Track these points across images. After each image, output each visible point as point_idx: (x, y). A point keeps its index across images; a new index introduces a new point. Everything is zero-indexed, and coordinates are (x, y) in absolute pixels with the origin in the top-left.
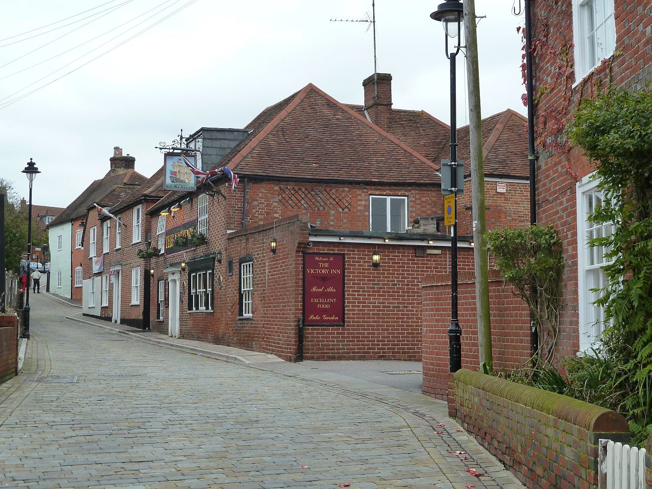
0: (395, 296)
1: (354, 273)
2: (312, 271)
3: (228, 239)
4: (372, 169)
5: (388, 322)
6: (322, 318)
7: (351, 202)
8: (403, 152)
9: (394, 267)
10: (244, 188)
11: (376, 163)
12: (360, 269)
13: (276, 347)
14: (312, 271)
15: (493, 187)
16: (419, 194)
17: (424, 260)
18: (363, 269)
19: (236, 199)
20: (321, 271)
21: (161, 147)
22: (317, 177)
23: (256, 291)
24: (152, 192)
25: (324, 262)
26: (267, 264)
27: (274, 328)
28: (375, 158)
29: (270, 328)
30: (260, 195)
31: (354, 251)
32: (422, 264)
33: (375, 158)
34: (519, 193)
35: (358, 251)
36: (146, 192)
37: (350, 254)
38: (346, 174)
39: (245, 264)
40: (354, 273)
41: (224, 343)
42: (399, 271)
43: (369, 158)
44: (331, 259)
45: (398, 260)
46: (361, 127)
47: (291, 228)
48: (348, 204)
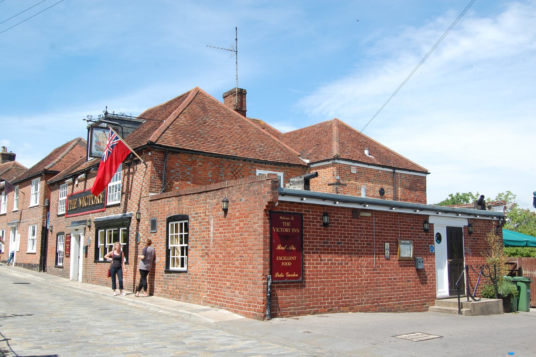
1: (309, 232)
2: (277, 230)
3: (150, 201)
4: (257, 151)
5: (334, 278)
6: (285, 275)
15: (348, 169)
16: (290, 172)
17: (358, 222)
19: (157, 167)
21: (89, 119)
34: (363, 175)
35: (312, 212)
36: (46, 168)
39: (174, 223)
44: (292, 219)
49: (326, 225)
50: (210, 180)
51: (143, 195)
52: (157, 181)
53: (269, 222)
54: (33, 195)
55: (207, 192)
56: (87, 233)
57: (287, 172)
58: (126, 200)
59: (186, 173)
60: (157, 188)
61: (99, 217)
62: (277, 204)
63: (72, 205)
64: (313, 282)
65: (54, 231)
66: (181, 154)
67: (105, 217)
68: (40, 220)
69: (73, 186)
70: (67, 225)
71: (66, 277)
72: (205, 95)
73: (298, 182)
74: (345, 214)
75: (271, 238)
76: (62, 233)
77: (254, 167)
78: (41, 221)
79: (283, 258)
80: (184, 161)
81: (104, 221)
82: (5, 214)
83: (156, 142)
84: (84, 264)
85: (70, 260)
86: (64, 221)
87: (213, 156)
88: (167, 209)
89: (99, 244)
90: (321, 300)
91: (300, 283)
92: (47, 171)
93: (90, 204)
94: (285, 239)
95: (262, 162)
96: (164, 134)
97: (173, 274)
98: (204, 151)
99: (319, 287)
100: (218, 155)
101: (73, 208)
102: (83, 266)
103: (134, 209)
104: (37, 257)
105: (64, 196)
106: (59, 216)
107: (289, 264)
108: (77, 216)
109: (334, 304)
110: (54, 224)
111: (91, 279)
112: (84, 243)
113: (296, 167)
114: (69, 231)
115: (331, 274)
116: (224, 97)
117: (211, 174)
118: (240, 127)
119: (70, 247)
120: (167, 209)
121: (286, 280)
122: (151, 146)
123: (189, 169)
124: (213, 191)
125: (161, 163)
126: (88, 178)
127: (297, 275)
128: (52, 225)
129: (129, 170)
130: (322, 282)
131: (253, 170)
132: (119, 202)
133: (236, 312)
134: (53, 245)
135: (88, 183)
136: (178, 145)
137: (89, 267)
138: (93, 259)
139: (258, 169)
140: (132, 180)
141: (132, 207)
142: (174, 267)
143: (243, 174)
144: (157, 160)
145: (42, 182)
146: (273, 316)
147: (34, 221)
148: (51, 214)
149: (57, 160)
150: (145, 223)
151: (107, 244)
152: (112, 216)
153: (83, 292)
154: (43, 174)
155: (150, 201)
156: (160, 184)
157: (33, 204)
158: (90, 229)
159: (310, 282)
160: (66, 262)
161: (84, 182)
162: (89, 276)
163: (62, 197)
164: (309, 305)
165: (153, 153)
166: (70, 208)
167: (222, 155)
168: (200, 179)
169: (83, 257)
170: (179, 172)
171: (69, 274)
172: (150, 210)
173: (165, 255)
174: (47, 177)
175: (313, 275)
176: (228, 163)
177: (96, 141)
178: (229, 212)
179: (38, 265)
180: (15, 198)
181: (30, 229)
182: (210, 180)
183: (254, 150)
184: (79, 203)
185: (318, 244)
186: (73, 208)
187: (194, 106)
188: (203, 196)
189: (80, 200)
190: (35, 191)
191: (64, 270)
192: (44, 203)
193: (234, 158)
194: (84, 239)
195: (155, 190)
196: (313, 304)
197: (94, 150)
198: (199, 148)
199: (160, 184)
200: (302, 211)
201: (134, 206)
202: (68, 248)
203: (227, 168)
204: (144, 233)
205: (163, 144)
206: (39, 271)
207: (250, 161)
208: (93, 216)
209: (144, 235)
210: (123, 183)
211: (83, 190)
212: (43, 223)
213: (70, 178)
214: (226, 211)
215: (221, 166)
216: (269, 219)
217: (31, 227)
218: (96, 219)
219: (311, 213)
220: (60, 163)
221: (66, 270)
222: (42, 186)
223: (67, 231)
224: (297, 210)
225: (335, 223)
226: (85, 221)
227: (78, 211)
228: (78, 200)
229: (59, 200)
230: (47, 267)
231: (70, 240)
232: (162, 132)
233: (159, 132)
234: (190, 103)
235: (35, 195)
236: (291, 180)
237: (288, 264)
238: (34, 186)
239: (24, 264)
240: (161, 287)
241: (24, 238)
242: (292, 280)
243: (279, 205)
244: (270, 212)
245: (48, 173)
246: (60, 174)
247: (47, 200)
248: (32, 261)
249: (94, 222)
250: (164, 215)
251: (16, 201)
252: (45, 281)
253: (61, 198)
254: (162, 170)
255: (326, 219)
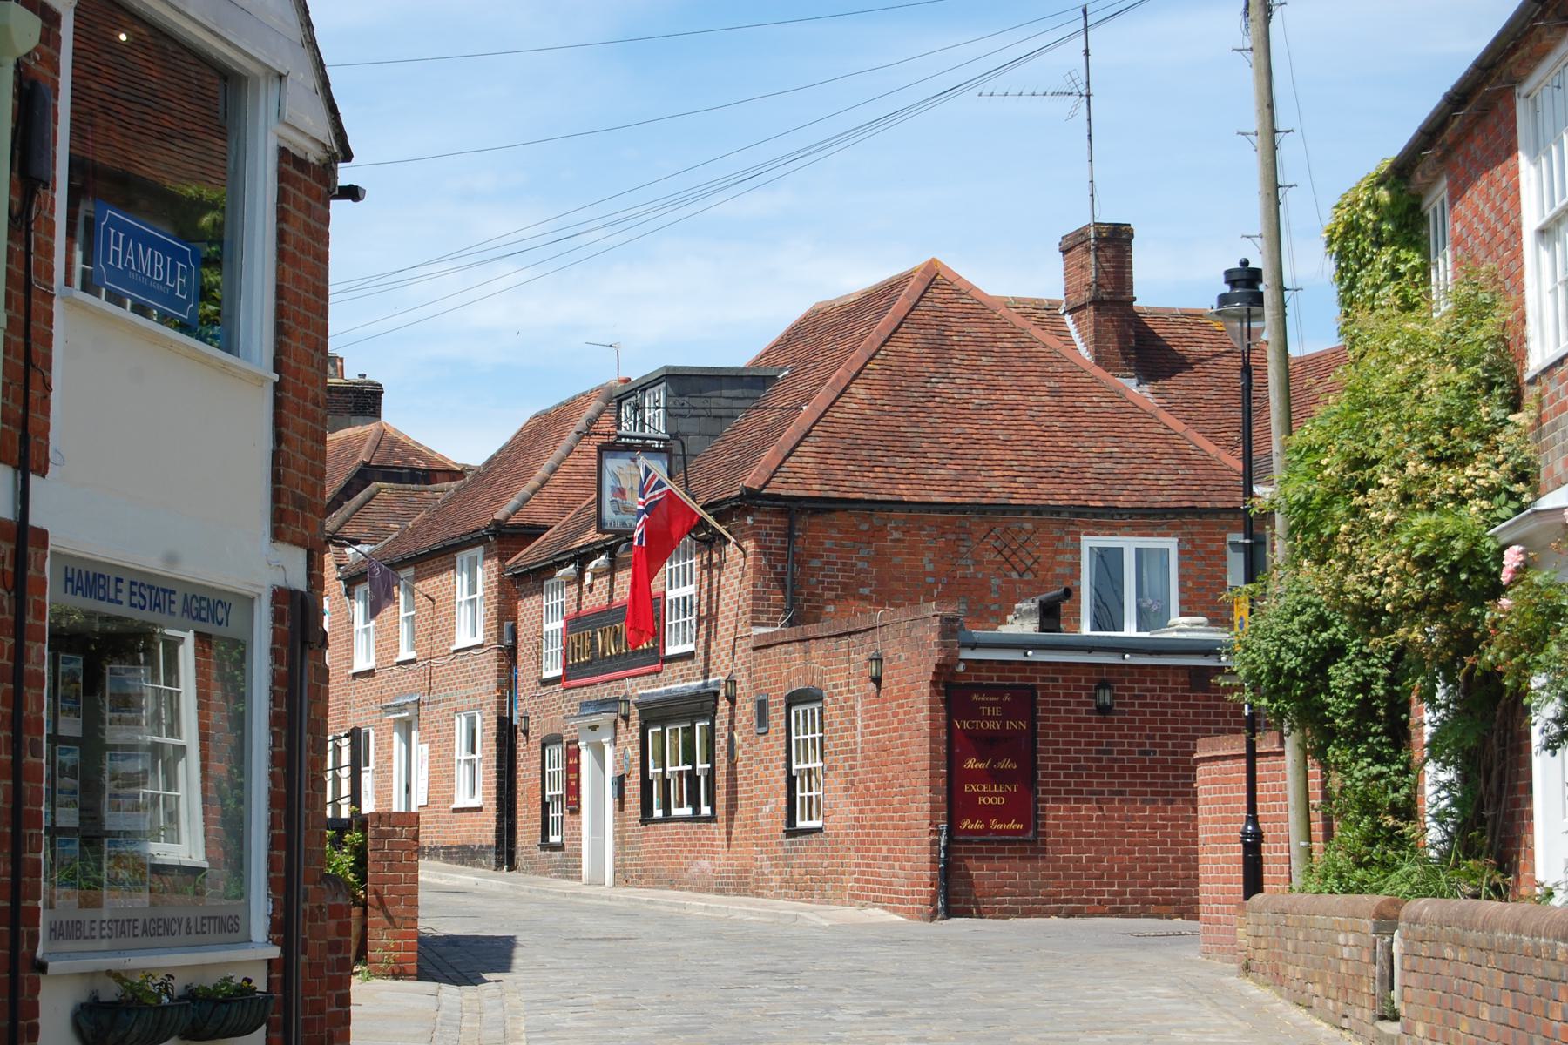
0: (1145, 777)
1: (1056, 727)
2: (966, 725)
3: (755, 649)
4: (1088, 475)
5: (1132, 835)
6: (987, 825)
7: (1039, 557)
8: (1162, 431)
9: (1144, 713)
10: (791, 528)
11: (1097, 460)
12: (1069, 719)
13: (884, 891)
14: (966, 725)
17: (1208, 699)
18: (1077, 720)
19: (770, 554)
20: (985, 725)
22: (958, 500)
23: (830, 768)
24: (516, 510)
25: (992, 704)
26: (859, 708)
27: (879, 850)
28: (1094, 449)
29: (868, 850)
30: (828, 544)
31: (1056, 680)
32: (1205, 707)
33: (1094, 449)
37: (1047, 687)
38: (1027, 491)
40: (1056, 727)
41: (745, 890)
42: (1155, 722)
43: (1080, 449)
44: (1007, 698)
45: (1152, 698)
46: (1060, 370)
47: (918, 632)
48: (1032, 560)
49: (1104, 710)
50: (930, 580)
51: (740, 632)
52: (771, 593)
53: (945, 708)
54: (462, 608)
55: (850, 634)
56: (621, 738)
57: (1192, 534)
58: (707, 642)
59: (854, 565)
60: (774, 613)
61: (649, 688)
62: (961, 668)
63: (579, 649)
64: (1065, 843)
65: (533, 733)
66: (837, 514)
67: (662, 689)
68: (490, 693)
69: (581, 588)
70: (569, 711)
71: (572, 878)
72: (958, 284)
73: (1029, 613)
74: (1166, 682)
75: (950, 744)
76: (555, 739)
77: (1072, 528)
78: (493, 699)
79: (981, 788)
80: (847, 532)
81: (658, 701)
82: (370, 673)
83: (764, 487)
84: (618, 832)
85: (580, 823)
86: (560, 698)
87: (935, 511)
88: (785, 671)
89: (651, 770)
90: (1090, 885)
91: (1031, 845)
92: (504, 527)
93: (624, 651)
94: (987, 744)
95: (1097, 512)
96: (792, 459)
97: (799, 839)
98: (906, 499)
99: (1084, 856)
100: (950, 508)
101: (582, 660)
102: (615, 838)
103: (723, 670)
104: (487, 820)
105: (557, 620)
106: (545, 683)
107: (998, 801)
108: (595, 684)
109: (1128, 896)
110: (533, 709)
111: (634, 875)
112: (615, 768)
113: (1222, 516)
114: (575, 731)
115: (1122, 826)
116: (1065, 251)
117: (931, 561)
118: (1054, 392)
119: (578, 780)
120: (785, 671)
121: (990, 837)
122: (751, 500)
123: (863, 553)
124: (860, 632)
125: (782, 542)
126: (619, 569)
127: (1020, 826)
128: (526, 712)
129: (710, 559)
130: (1094, 843)
131: (1068, 539)
132: (690, 647)
133: (895, 911)
134: (533, 776)
135: (618, 584)
136: (827, 488)
137: (630, 837)
138: (637, 814)
139: (1086, 534)
140: (718, 588)
141: (718, 661)
142: (810, 819)
143: (1036, 555)
144: (771, 535)
145: (489, 562)
146: (950, 913)
147: (471, 699)
148: (521, 677)
149: (534, 483)
150: (746, 708)
151: (669, 769)
152: (678, 686)
153: (606, 902)
154: (490, 538)
155: (755, 649)
156: (782, 600)
157: (463, 639)
158: (627, 726)
159: (1057, 843)
160: (570, 829)
161: (608, 577)
162: (631, 865)
163: (552, 621)
164: (1054, 895)
165: (759, 517)
166: (573, 660)
167: (961, 504)
168: (898, 579)
169: (615, 809)
170: (835, 563)
171: (580, 866)
172: (755, 672)
173: (784, 791)
174: (505, 549)
175: (1065, 826)
176: (986, 526)
177: (612, 487)
178: (884, 683)
179: (489, 847)
180: (403, 614)
181: (461, 724)
182: (930, 580)
183: (1080, 475)
184: (597, 643)
185: (1082, 756)
186: (582, 660)
187: (906, 338)
188: (844, 641)
189: (599, 634)
190: (469, 595)
191: (567, 855)
192: (500, 635)
193: (1004, 509)
194: (615, 757)
195: (768, 619)
196: (1067, 893)
197: (609, 514)
198: (892, 491)
199: (782, 600)
200: (1035, 679)
201: (722, 662)
202: (573, 784)
203: (982, 540)
204: (744, 735)
205: (783, 492)
206: (494, 867)
207: (1058, 514)
208: (634, 687)
209: (744, 740)
210: (700, 594)
211: (605, 603)
212: (501, 707)
213: (571, 561)
214: (877, 680)
215: (962, 536)
216: (943, 701)
217: (464, 719)
218: (641, 696)
219: (1060, 683)
220: (545, 492)
221: (572, 856)
222: (489, 578)
223: (569, 732)
224: (999, 678)
225: (1133, 705)
226: (616, 701)
227: (597, 670)
228: (594, 633)
229: (545, 631)
230: (520, 851)
231: (579, 759)
232: (786, 451)
233: (775, 453)
234: (895, 331)
235: (468, 608)
236: (1017, 606)
237: (994, 800)
238: (465, 576)
239: (447, 848)
240: (780, 874)
241: (443, 756)
242: (1007, 837)
243: (967, 669)
244: (946, 686)
245: (504, 533)
246: (543, 542)
247: (508, 624)
248: (470, 836)
249: (637, 705)
250: (780, 689)
251: (405, 624)
252: (511, 887)
253: (547, 623)
254: (787, 561)
255: (1105, 697)
